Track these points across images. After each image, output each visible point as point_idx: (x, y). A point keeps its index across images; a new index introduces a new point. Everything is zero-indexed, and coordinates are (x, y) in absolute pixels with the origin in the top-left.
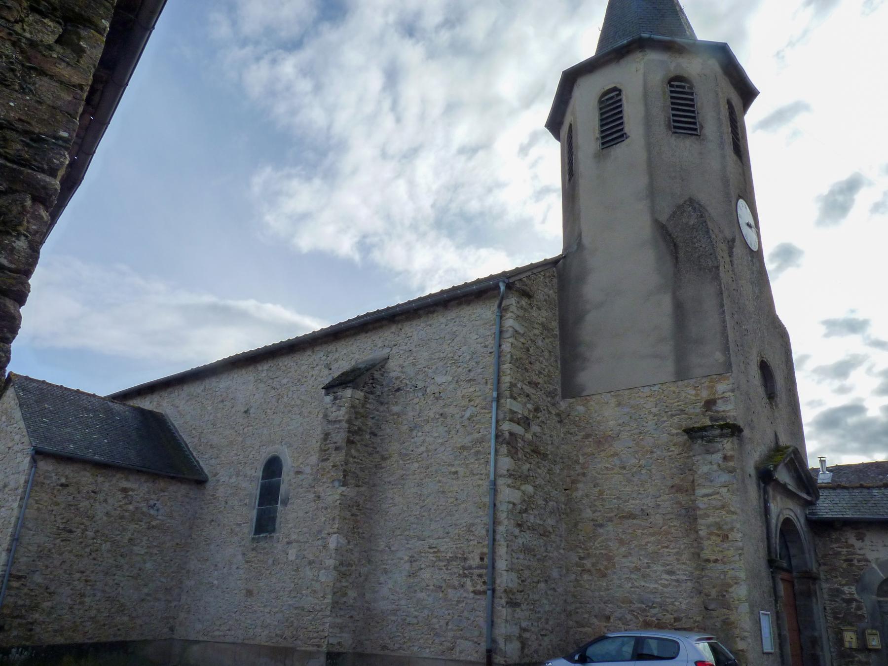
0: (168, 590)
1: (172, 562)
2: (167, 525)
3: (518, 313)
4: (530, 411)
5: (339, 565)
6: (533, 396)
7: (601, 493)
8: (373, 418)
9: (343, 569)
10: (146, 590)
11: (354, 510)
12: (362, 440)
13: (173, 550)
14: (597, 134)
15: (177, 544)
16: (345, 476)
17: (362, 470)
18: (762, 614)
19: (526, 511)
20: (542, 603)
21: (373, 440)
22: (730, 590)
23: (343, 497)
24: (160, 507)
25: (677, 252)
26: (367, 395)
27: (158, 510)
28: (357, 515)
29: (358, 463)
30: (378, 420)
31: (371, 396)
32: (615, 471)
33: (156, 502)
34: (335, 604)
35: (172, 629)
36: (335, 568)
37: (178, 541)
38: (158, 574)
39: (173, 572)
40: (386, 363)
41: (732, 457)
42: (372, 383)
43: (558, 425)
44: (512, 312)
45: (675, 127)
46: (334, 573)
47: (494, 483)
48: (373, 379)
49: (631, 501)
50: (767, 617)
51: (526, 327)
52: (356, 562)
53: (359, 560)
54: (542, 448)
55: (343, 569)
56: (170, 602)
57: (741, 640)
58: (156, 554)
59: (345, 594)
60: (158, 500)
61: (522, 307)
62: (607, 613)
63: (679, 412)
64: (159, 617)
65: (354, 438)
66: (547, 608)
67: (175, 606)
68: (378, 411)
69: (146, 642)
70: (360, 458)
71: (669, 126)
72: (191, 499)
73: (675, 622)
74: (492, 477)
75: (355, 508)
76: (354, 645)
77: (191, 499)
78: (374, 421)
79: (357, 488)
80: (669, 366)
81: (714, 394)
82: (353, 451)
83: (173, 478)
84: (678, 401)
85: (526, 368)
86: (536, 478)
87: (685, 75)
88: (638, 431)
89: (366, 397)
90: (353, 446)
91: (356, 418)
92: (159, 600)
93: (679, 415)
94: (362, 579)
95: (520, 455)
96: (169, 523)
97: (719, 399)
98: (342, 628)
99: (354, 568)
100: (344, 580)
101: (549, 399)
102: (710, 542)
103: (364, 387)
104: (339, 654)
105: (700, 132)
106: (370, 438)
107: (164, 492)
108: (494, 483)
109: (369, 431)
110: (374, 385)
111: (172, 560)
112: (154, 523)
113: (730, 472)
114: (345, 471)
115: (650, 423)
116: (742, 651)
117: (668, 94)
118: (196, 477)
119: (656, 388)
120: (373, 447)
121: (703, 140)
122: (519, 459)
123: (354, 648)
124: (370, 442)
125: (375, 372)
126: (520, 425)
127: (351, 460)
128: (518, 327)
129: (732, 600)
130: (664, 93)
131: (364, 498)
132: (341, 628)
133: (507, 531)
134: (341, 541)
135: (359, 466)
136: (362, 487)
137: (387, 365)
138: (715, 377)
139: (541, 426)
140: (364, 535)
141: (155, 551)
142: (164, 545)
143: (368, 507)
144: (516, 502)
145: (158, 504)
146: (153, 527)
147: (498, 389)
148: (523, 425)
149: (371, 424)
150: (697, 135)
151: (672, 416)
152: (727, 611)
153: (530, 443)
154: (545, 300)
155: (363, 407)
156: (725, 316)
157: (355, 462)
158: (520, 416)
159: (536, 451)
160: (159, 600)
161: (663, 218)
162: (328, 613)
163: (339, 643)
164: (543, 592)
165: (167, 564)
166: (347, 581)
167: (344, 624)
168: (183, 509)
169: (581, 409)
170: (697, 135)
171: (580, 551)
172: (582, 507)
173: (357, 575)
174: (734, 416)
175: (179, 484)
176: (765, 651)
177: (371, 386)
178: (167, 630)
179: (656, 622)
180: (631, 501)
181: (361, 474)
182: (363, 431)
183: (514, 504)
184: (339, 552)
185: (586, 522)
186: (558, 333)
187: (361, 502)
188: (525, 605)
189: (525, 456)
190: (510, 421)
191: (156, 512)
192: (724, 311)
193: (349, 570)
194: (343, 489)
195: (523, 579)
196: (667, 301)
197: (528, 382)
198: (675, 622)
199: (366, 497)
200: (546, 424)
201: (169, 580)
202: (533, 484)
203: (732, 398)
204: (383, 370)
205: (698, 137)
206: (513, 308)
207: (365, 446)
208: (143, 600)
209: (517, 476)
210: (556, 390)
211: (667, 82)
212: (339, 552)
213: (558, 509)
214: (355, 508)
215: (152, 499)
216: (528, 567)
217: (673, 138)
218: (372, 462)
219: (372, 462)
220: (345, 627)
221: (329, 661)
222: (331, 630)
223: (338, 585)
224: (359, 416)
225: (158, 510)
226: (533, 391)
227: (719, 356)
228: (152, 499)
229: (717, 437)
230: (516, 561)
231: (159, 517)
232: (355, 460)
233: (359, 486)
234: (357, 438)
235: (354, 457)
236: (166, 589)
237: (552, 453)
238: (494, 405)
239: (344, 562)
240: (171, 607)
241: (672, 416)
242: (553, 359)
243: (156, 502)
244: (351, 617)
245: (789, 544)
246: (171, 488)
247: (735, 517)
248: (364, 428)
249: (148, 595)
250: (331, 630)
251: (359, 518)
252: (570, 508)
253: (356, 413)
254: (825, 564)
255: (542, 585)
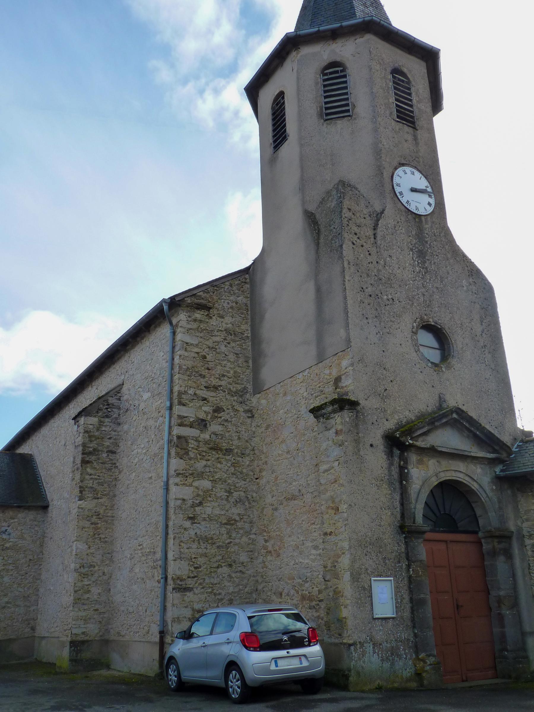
0: (26, 598)
1: (28, 575)
2: (20, 545)
3: (190, 326)
4: (207, 413)
5: (80, 567)
6: (211, 399)
7: (276, 478)
8: (110, 438)
9: (83, 570)
10: (6, 599)
11: (94, 519)
12: (99, 459)
13: (26, 565)
14: (271, 141)
15: (30, 560)
16: (81, 492)
17: (100, 484)
18: (374, 580)
19: (200, 504)
20: (223, 585)
21: (111, 457)
22: (339, 560)
23: (80, 510)
24: (11, 531)
25: (318, 239)
26: (102, 419)
27: (9, 534)
28: (98, 523)
29: (96, 479)
30: (115, 439)
31: (107, 420)
32: (284, 457)
33: (7, 528)
34: (77, 601)
35: (33, 629)
36: (76, 570)
37: (31, 557)
38: (15, 586)
39: (29, 583)
40: (121, 389)
41: (341, 430)
42: (107, 409)
43: (249, 421)
44: (181, 327)
45: (327, 114)
46: (76, 575)
47: (167, 484)
48: (108, 405)
49: (294, 483)
50: (389, 583)
51: (201, 337)
52: (99, 563)
53: (103, 561)
54: (224, 444)
55: (83, 570)
56: (29, 607)
57: (344, 608)
58: (12, 570)
59: (89, 591)
60: (9, 526)
61: (195, 320)
62: (280, 590)
63: (319, 393)
64: (20, 620)
65: (90, 458)
66: (231, 589)
67: (33, 610)
68: (115, 431)
69: (10, 640)
70: (98, 474)
71: (320, 115)
72: (39, 522)
73: (319, 594)
74: (165, 479)
75: (95, 517)
76: (101, 633)
77: (39, 522)
78: (111, 441)
79: (96, 500)
80: (313, 351)
81: (340, 371)
82: (89, 470)
83: (19, 507)
84: (320, 383)
85: (201, 375)
86: (216, 472)
87: (338, 59)
88: (296, 416)
89: (100, 421)
90: (88, 465)
91: (91, 441)
92: (18, 606)
93: (320, 396)
94: (105, 578)
95: (191, 455)
96: (21, 544)
97: (343, 375)
98: (86, 620)
99: (97, 568)
100: (86, 580)
101: (235, 398)
102: (328, 516)
103: (97, 412)
104: (83, 642)
105: (352, 113)
106: (108, 455)
107: (14, 519)
108: (167, 484)
109: (105, 450)
110: (109, 410)
111: (27, 574)
112: (7, 545)
113: (340, 445)
114: (80, 487)
115: (303, 407)
116: (345, 618)
117: (320, 81)
118: (39, 504)
119: (306, 373)
120: (112, 464)
121: (355, 119)
122: (190, 459)
123: (101, 636)
124: (108, 460)
125: (110, 399)
126: (193, 428)
127: (87, 477)
128: (188, 339)
129: (340, 569)
130: (317, 84)
131: (104, 508)
132: (85, 620)
133: (174, 524)
134: (81, 547)
135: (97, 481)
136: (101, 498)
137: (122, 390)
138: (341, 353)
139: (223, 425)
140: (106, 539)
141: (11, 567)
142: (18, 562)
143: (109, 515)
144: (185, 497)
145: (9, 530)
146: (7, 548)
147: (171, 399)
148: (197, 427)
149: (108, 444)
150: (349, 116)
151: (316, 397)
152: (337, 580)
153: (206, 443)
154: (232, 308)
155: (98, 430)
156: (346, 293)
157: (92, 478)
158: (191, 420)
159: (216, 448)
160: (18, 606)
161: (312, 208)
162: (71, 608)
163: (83, 633)
164: (226, 575)
165: (23, 577)
166: (90, 580)
167: (89, 616)
168: (33, 531)
169: (263, 402)
170: (349, 116)
171: (265, 534)
172: (265, 493)
173: (101, 574)
174: (352, 390)
175: (27, 511)
176: (376, 616)
177: (105, 411)
178: (29, 630)
179: (308, 594)
180: (294, 483)
181: (99, 488)
182: (98, 451)
183: (184, 500)
184: (78, 556)
185: (268, 507)
186: (249, 335)
187: (102, 512)
188: (199, 589)
189: (200, 455)
190: (180, 425)
191: (8, 536)
192: (345, 288)
193: (91, 571)
194: (80, 502)
195: (196, 566)
196: (311, 286)
197: (205, 387)
198: (319, 594)
199: (106, 506)
200: (231, 422)
201: (26, 589)
202: (212, 479)
203: (351, 372)
204: (119, 395)
205: (350, 118)
206: (183, 323)
207: (102, 463)
208: (4, 607)
209: (187, 474)
210: (245, 388)
211: (320, 72)
212: (78, 556)
213: (248, 498)
214: (95, 517)
215: (3, 526)
216: (205, 555)
217: (325, 125)
218: (112, 476)
219: (112, 476)
220: (90, 619)
221: (73, 648)
222: (74, 623)
223: (79, 584)
224: (93, 439)
225: (9, 534)
226: (213, 394)
227: (342, 333)
228: (3, 526)
229: (330, 413)
230: (187, 551)
231: (11, 540)
232: (91, 477)
233: (98, 498)
234: (93, 458)
235: (90, 475)
236: (24, 597)
237: (238, 447)
238: (167, 413)
239: (85, 565)
240: (30, 611)
241: (316, 397)
242: (241, 361)
243: (7, 528)
244: (96, 610)
245: (474, 505)
246: (20, 515)
247: (342, 489)
248: (100, 448)
249: (7, 603)
250: (74, 623)
251: (99, 525)
252: (259, 495)
253: (90, 437)
254: (527, 520)
255: (225, 570)
